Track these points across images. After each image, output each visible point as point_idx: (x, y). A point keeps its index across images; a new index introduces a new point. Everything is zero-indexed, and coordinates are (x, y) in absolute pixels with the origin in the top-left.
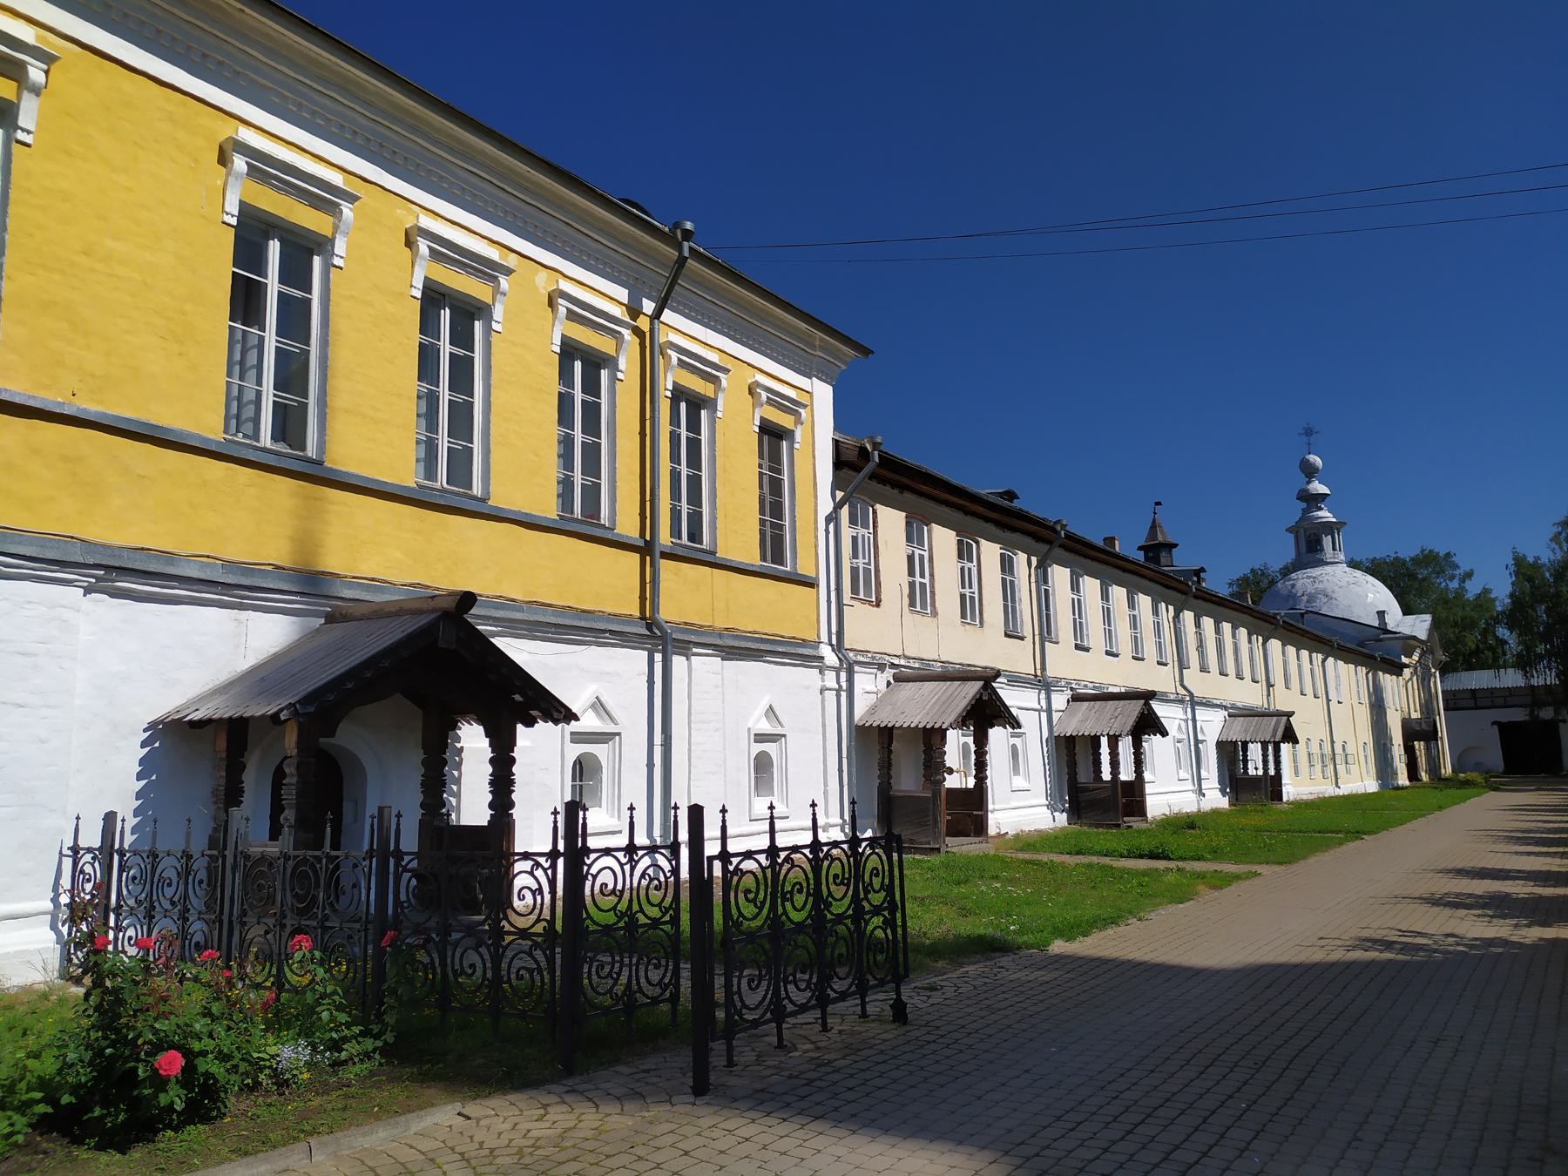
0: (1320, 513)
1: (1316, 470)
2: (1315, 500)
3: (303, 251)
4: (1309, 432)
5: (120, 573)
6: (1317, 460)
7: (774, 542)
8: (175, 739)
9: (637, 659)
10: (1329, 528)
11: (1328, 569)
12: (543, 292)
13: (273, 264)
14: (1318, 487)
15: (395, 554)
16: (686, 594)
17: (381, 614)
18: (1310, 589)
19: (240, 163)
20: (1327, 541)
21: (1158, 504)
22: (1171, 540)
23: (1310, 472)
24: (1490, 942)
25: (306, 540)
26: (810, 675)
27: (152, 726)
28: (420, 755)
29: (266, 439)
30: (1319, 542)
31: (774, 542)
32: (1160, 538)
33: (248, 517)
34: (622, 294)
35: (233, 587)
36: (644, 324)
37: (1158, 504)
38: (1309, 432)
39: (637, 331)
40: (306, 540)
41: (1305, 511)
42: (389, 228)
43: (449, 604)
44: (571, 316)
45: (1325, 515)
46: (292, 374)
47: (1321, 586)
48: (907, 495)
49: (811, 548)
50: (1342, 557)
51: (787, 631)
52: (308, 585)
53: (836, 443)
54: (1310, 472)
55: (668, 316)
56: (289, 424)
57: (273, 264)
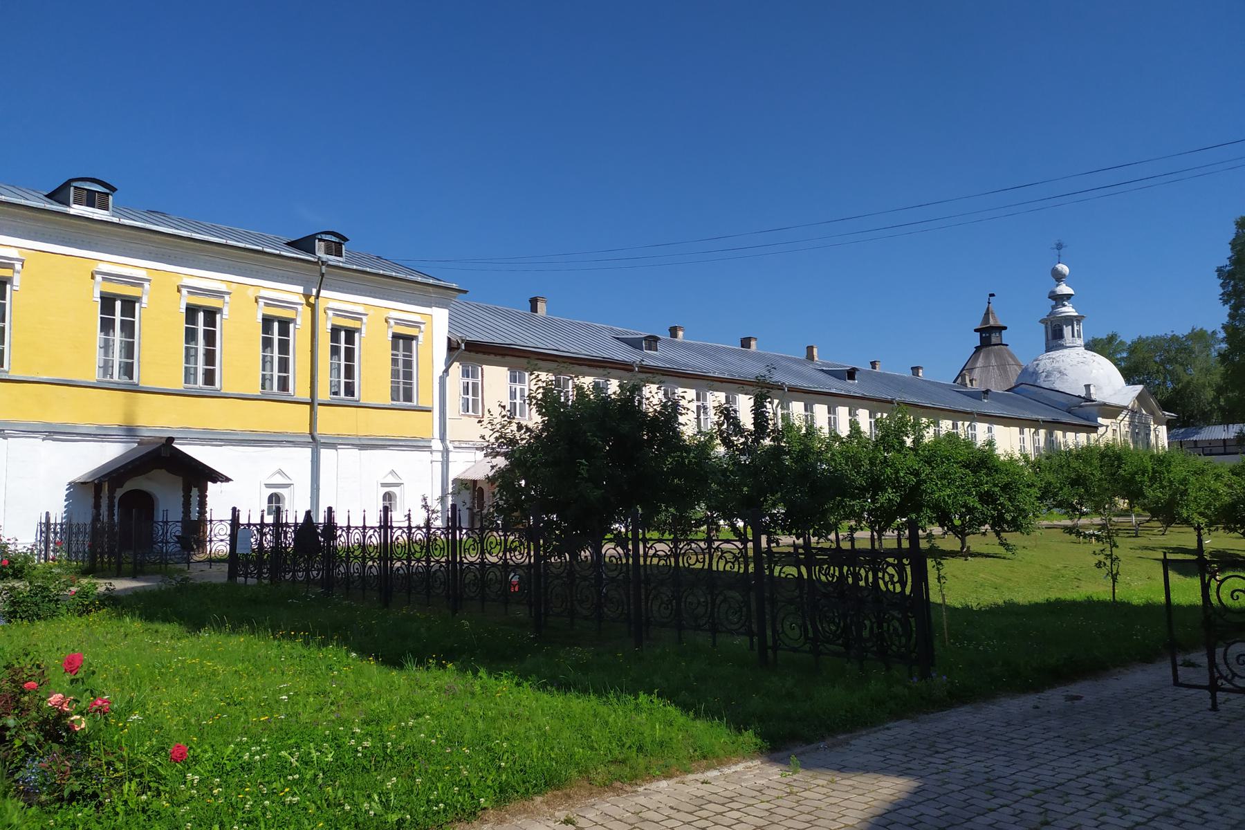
0: (1064, 309)
1: (1064, 276)
2: (1060, 299)
3: (129, 305)
4: (1059, 246)
5: (53, 433)
6: (1064, 268)
7: (403, 391)
8: (76, 488)
9: (307, 452)
10: (1070, 320)
11: (1066, 351)
12: (245, 299)
13: (118, 310)
14: (1064, 289)
15: (159, 418)
16: (331, 421)
17: (149, 443)
18: (1049, 368)
19: (99, 278)
20: (1067, 330)
21: (992, 295)
22: (1001, 324)
23: (1059, 277)
24: (126, 590)
25: (129, 414)
26: (425, 455)
27: (73, 485)
28: (181, 493)
29: (116, 377)
30: (1061, 330)
31: (403, 391)
32: (992, 322)
33: (108, 409)
34: (300, 289)
35: (100, 435)
36: (312, 300)
37: (992, 295)
38: (1059, 246)
39: (308, 304)
40: (129, 414)
41: (1054, 308)
42: (165, 288)
43: (164, 441)
44: (266, 304)
45: (1069, 310)
46: (129, 350)
47: (1056, 365)
48: (508, 359)
49: (425, 392)
50: (1080, 342)
51: (409, 435)
52: (130, 431)
53: (449, 339)
54: (1059, 277)
55: (323, 293)
56: (128, 370)
57: (118, 310)
